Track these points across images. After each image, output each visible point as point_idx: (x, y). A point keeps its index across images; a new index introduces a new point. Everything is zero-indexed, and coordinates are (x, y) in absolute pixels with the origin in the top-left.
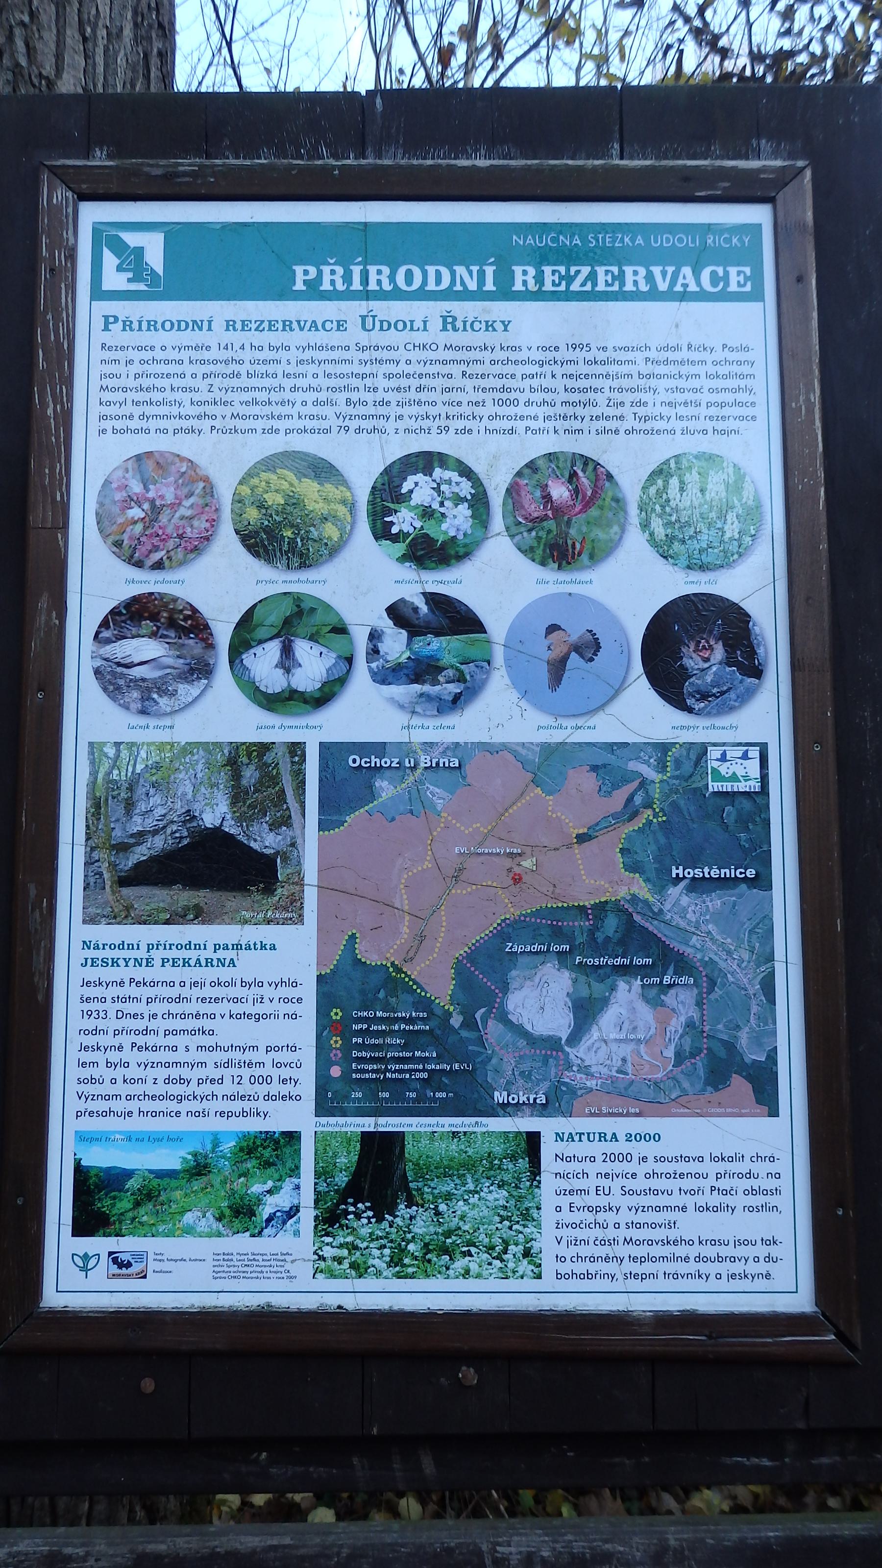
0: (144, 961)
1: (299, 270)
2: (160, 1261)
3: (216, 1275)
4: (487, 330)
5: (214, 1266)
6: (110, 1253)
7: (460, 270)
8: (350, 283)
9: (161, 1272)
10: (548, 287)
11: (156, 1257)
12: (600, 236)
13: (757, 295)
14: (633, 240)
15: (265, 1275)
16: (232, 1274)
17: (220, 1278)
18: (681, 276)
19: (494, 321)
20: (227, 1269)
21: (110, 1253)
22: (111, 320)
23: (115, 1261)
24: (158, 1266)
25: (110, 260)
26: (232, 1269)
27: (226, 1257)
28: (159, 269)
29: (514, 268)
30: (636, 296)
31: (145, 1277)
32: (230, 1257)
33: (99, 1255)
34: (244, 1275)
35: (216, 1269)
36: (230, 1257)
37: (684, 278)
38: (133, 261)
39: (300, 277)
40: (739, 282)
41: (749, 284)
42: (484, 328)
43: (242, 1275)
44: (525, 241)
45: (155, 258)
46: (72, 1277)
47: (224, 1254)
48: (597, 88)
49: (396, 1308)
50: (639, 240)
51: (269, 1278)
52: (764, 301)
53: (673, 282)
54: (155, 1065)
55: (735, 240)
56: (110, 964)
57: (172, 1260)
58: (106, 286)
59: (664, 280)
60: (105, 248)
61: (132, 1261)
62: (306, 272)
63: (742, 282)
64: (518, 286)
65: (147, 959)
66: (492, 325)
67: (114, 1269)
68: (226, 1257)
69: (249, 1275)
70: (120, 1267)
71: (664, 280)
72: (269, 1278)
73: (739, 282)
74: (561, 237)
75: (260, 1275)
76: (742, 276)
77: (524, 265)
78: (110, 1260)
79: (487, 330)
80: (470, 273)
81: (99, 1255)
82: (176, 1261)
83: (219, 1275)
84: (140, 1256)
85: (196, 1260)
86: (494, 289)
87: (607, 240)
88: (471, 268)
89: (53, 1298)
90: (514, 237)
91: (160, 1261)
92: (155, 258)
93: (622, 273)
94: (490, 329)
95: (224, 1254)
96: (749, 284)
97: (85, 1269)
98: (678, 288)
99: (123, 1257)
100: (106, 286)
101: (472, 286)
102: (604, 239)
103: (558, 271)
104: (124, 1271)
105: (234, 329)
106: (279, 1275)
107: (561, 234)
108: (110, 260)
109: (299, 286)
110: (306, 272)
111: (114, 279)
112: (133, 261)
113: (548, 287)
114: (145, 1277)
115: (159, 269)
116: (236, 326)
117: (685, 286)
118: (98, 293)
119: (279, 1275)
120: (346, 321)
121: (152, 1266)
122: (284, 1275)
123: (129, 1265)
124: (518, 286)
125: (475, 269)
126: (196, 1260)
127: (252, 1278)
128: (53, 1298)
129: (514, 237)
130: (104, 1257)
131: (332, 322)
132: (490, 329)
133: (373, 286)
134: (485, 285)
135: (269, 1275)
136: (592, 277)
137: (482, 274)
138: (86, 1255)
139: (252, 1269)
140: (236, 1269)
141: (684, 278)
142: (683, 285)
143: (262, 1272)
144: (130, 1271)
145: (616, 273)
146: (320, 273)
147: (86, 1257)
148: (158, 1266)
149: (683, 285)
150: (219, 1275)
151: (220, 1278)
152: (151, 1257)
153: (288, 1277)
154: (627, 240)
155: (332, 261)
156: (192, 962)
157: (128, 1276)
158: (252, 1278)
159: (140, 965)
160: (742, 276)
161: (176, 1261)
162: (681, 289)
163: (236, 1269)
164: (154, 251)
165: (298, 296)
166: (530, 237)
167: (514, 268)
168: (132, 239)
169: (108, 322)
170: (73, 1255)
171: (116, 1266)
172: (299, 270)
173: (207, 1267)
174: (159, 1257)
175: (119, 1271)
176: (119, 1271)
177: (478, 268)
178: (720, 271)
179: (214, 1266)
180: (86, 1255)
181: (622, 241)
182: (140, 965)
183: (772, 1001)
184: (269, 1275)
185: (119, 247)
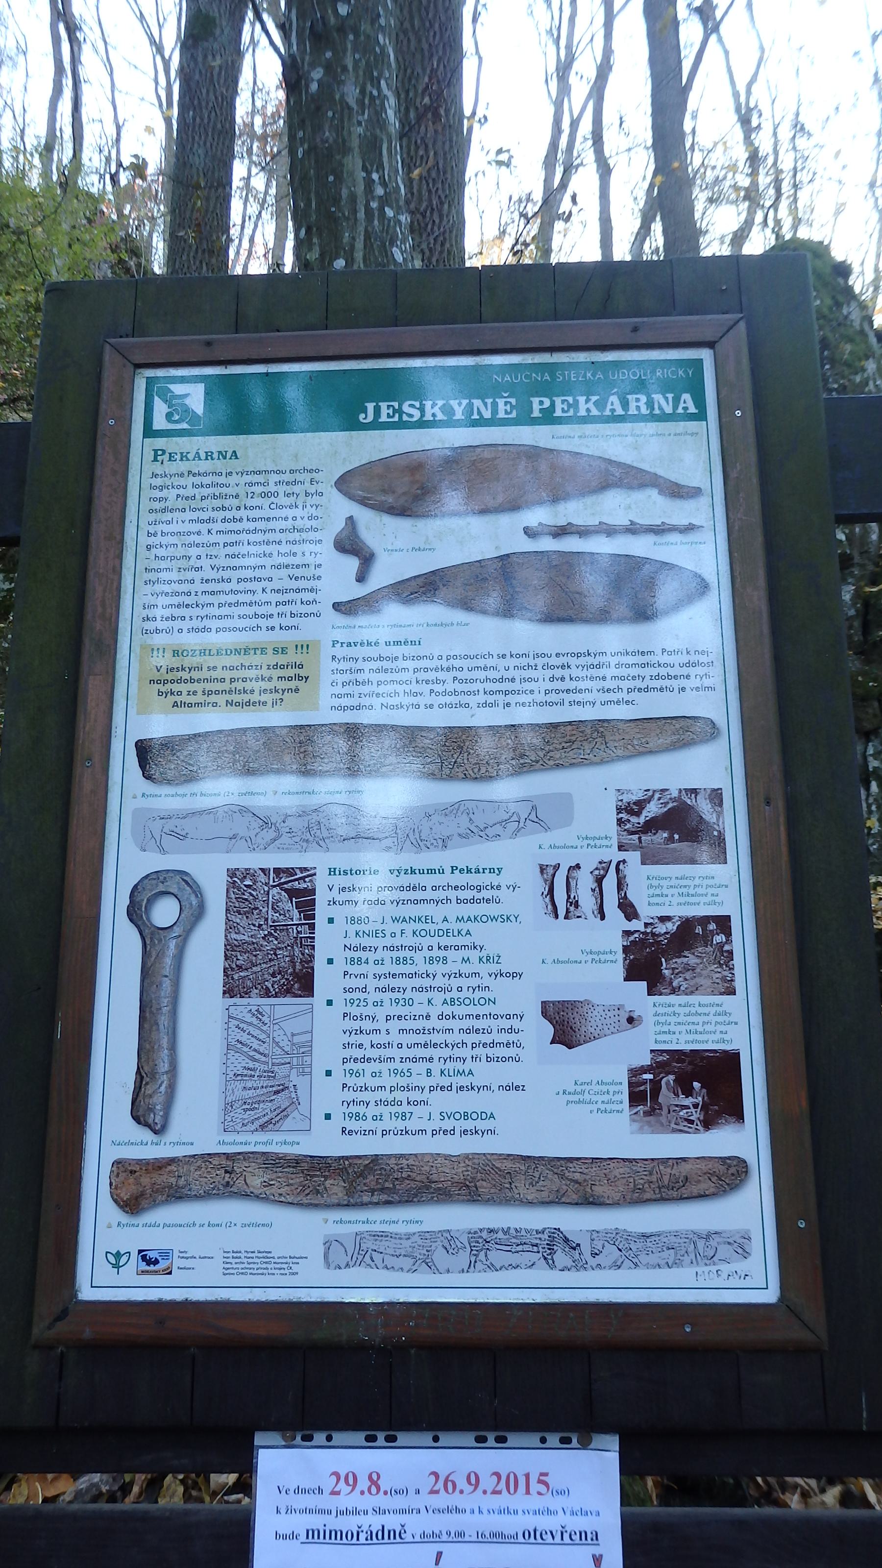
1: (535, 401)
6: (140, 1251)
7: (477, 403)
9: (184, 1268)
10: (501, 415)
11: (182, 1255)
13: (701, 415)
14: (593, 375)
15: (270, 1271)
16: (241, 1271)
18: (682, 401)
20: (235, 1266)
21: (140, 1251)
22: (160, 453)
23: (144, 1258)
25: (160, 408)
27: (235, 1255)
29: (366, 404)
30: (639, 418)
31: (170, 1273)
32: (238, 1255)
33: (107, 1253)
34: (251, 1271)
36: (238, 1255)
37: (685, 402)
39: (536, 407)
40: (563, 409)
41: (514, 412)
44: (542, 378)
46: (105, 1274)
48: (652, 261)
50: (547, 377)
52: (706, 420)
53: (675, 407)
54: (417, 1018)
55: (680, 372)
59: (668, 403)
60: (156, 398)
61: (159, 1259)
62: (541, 403)
63: (391, 414)
67: (143, 1266)
68: (235, 1255)
70: (148, 1264)
71: (668, 403)
73: (563, 409)
75: (265, 1271)
76: (509, 406)
77: (637, 394)
80: (485, 404)
84: (166, 1254)
85: (205, 1257)
86: (697, 411)
88: (486, 400)
93: (576, 402)
96: (514, 412)
97: (117, 1266)
98: (607, 413)
99: (152, 1255)
101: (487, 414)
103: (510, 403)
104: (152, 1268)
105: (212, 459)
106: (282, 1271)
109: (536, 414)
110: (541, 403)
113: (501, 415)
114: (170, 1273)
116: (214, 456)
117: (686, 409)
121: (177, 1263)
122: (286, 1271)
123: (156, 1262)
125: (489, 401)
126: (205, 1257)
128: (86, 1293)
129: (534, 375)
133: (428, 417)
134: (554, 412)
135: (273, 1271)
136: (377, 411)
137: (495, 405)
141: (685, 402)
142: (683, 408)
144: (157, 1267)
145: (571, 402)
146: (553, 404)
147: (118, 1256)
149: (683, 408)
154: (589, 375)
155: (506, 395)
156: (464, 933)
157: (156, 1272)
160: (391, 409)
162: (682, 411)
163: (243, 1266)
165: (534, 422)
167: (366, 404)
168: (178, 389)
169: (157, 454)
170: (107, 1253)
172: (535, 401)
173: (218, 1264)
175: (148, 1268)
176: (148, 1268)
177: (491, 400)
178: (570, 399)
181: (585, 376)
183: (172, 1161)
184: (273, 1271)
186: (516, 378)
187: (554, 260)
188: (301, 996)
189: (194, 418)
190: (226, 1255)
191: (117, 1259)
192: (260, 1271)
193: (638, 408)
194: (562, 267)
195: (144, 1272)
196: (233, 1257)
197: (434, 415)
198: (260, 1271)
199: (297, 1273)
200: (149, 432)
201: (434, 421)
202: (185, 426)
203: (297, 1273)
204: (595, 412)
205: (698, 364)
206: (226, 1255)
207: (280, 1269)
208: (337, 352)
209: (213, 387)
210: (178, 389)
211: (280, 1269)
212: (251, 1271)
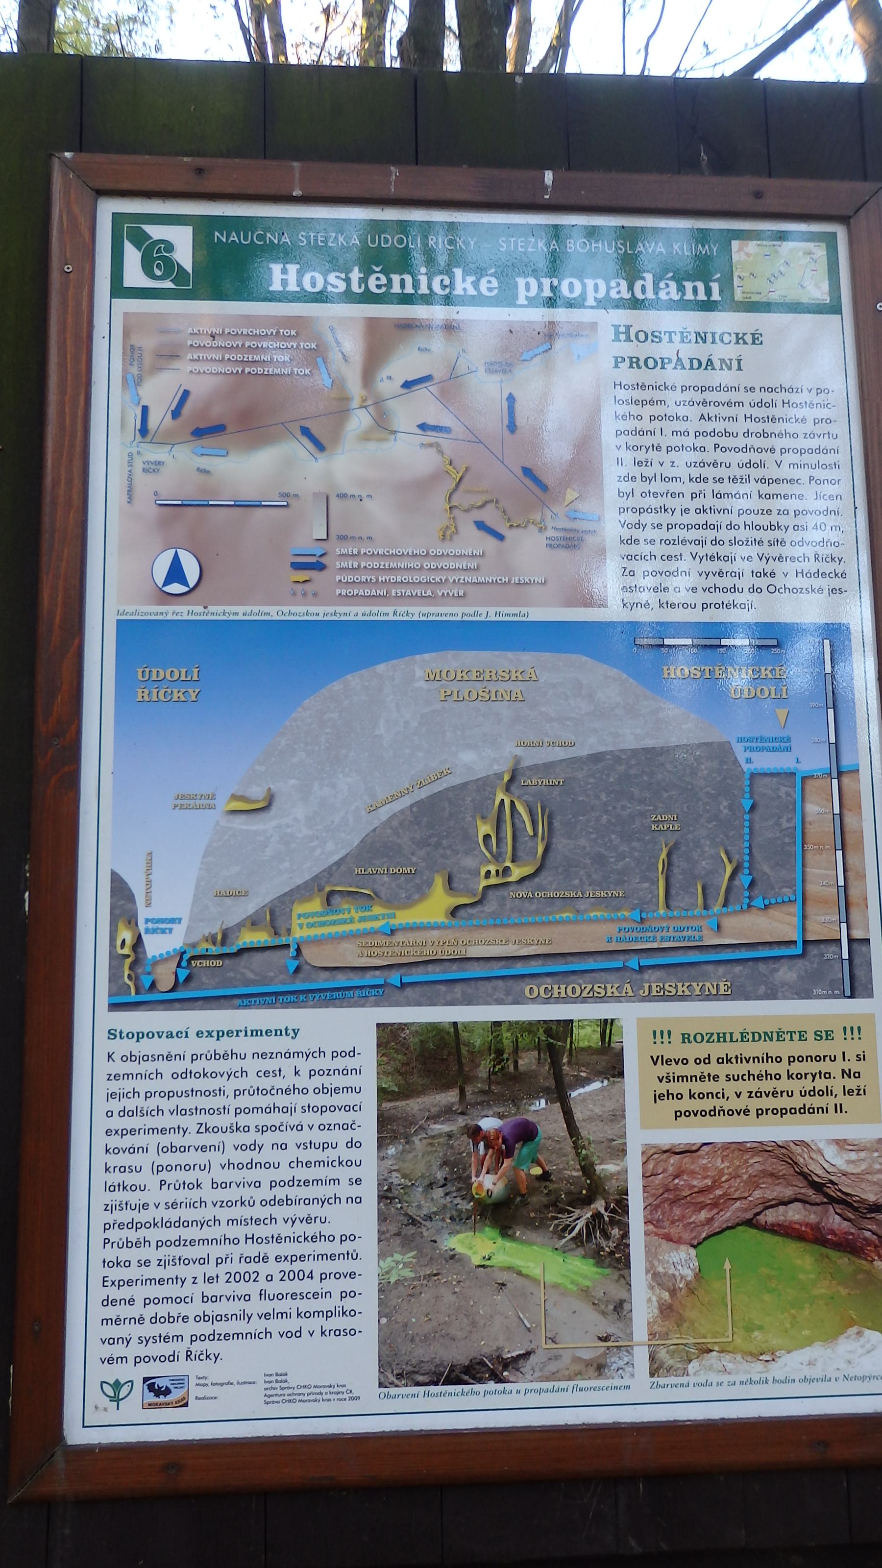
0: (775, 1035)
2: (204, 1385)
3: (268, 1400)
4: (737, 343)
5: (266, 1389)
6: (146, 1380)
8: (684, 294)
9: (204, 1398)
12: (512, 240)
13: (835, 309)
15: (325, 1397)
17: (273, 1402)
19: (744, 334)
20: (280, 1392)
23: (151, 1388)
24: (201, 1392)
25: (132, 256)
26: (286, 1392)
27: (279, 1378)
28: (188, 266)
31: (186, 1405)
33: (102, 1383)
34: (301, 1397)
35: (269, 1392)
38: (156, 257)
42: (734, 341)
43: (298, 1398)
44: (227, 239)
45: (184, 255)
47: (277, 1375)
49: (277, 1434)
51: (329, 1400)
56: (824, 1037)
57: (216, 1384)
58: (127, 283)
64: (276, 286)
65: (778, 1033)
66: (742, 338)
67: (151, 1398)
68: (279, 1378)
69: (306, 1398)
70: (157, 1395)
72: (329, 1400)
74: (269, 235)
75: (318, 1397)
78: (146, 1387)
79: (737, 343)
81: (132, 1381)
82: (222, 1384)
83: (271, 1399)
84: (180, 1381)
85: (245, 1383)
87: (520, 244)
89: (76, 1434)
90: (217, 234)
91: (204, 1385)
92: (184, 255)
94: (741, 341)
95: (277, 1375)
99: (162, 1383)
100: (127, 283)
102: (516, 242)
104: (162, 1399)
106: (340, 1396)
107: (269, 231)
108: (132, 256)
111: (134, 275)
112: (156, 257)
114: (186, 1405)
115: (188, 266)
118: (119, 290)
119: (340, 1396)
120: (761, 335)
121: (195, 1391)
122: (346, 1396)
123: (167, 1392)
124: (276, 286)
127: (310, 1401)
128: (76, 1434)
129: (217, 234)
130: (138, 1384)
131: (730, 334)
132: (741, 341)
135: (329, 1396)
138: (117, 1382)
139: (309, 1391)
140: (290, 1391)
143: (321, 1393)
144: (169, 1398)
147: (117, 1385)
148: (201, 1392)
150: (271, 1399)
151: (273, 1402)
152: (193, 1381)
153: (351, 1399)
157: (167, 1405)
158: (310, 1401)
159: (771, 1040)
161: (222, 1384)
164: (183, 245)
166: (234, 234)
168: (156, 232)
170: (102, 1383)
171: (152, 1394)
174: (202, 1382)
175: (156, 1400)
176: (156, 1400)
179: (266, 1389)
180: (117, 1382)
182: (771, 1040)
184: (329, 1396)
185: (139, 239)
186: (246, 239)
187: (571, 68)
188: (683, 998)
189: (180, 275)
190: (268, 1379)
191: (116, 1391)
192: (312, 1397)
193: (284, 282)
194: (580, 79)
195: (151, 1406)
196: (277, 1381)
197: (465, 289)
198: (312, 1397)
199: (359, 1398)
200: (119, 290)
201: (465, 295)
202: (168, 284)
203: (359, 1398)
204: (472, 291)
205: (834, 235)
206: (268, 1379)
207: (338, 1393)
208: (355, 192)
209: (204, 228)
210: (156, 232)
211: (338, 1393)
212: (301, 1397)
